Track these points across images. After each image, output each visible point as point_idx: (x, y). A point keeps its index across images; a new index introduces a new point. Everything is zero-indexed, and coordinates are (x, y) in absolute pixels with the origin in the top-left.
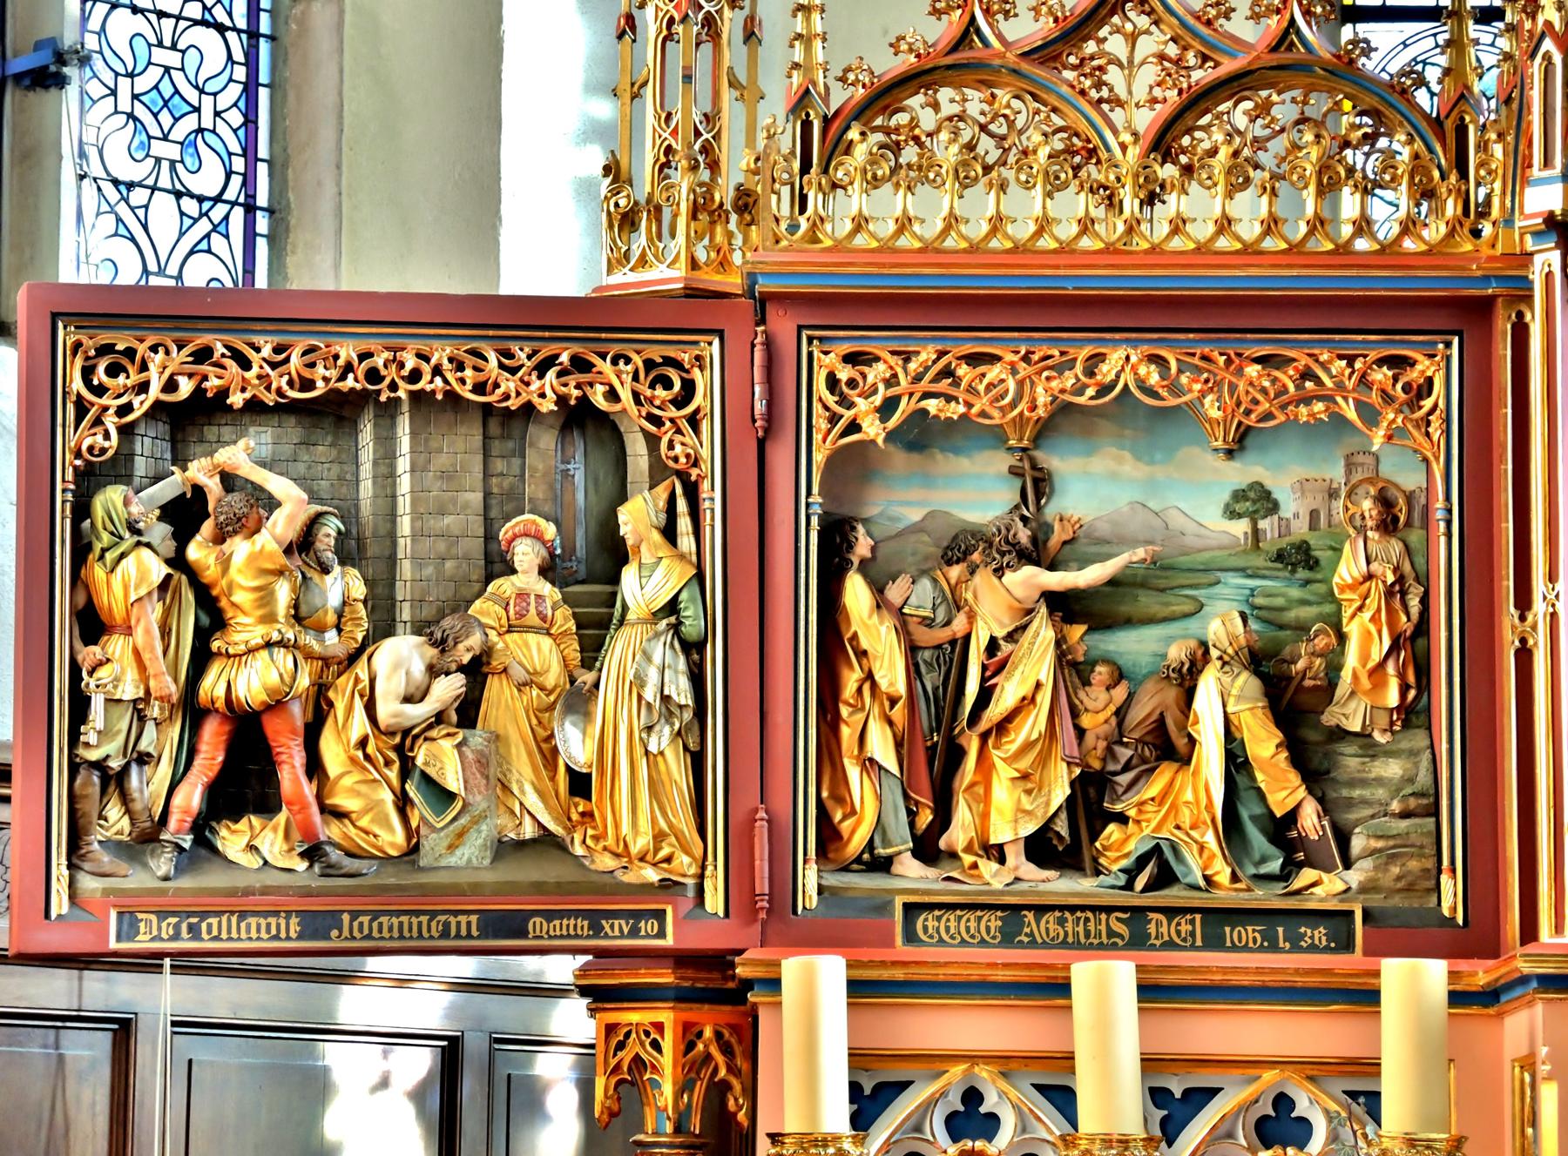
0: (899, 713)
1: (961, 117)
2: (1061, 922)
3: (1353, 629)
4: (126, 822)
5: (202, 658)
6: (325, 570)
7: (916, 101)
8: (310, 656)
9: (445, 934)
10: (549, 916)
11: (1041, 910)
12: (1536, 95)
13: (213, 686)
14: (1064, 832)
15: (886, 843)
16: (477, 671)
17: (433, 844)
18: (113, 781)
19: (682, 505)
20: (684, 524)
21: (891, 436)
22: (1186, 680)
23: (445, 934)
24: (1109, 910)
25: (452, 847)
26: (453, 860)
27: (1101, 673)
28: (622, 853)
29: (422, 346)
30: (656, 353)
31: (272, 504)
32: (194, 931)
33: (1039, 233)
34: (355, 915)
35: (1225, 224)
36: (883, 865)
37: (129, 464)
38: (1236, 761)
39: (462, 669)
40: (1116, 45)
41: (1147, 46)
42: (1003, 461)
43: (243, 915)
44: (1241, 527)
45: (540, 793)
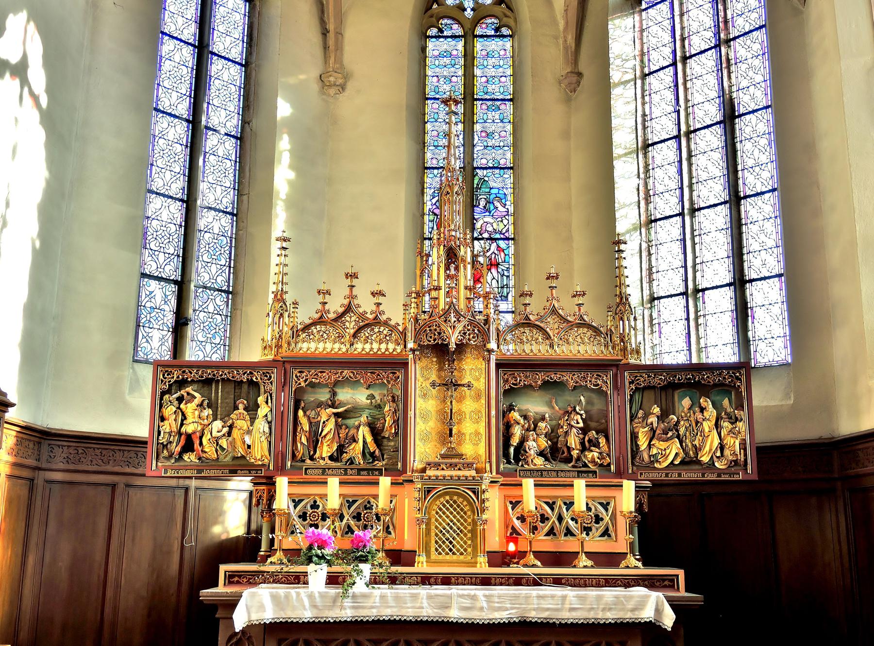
2: (332, 471)
3: (387, 419)
7: (313, 328)
8: (201, 424)
9: (222, 473)
10: (241, 470)
11: (329, 469)
16: (231, 427)
19: (269, 398)
24: (341, 469)
25: (225, 458)
38: (365, 442)
41: (353, 319)
42: (328, 390)
43: (186, 470)
44: (369, 401)
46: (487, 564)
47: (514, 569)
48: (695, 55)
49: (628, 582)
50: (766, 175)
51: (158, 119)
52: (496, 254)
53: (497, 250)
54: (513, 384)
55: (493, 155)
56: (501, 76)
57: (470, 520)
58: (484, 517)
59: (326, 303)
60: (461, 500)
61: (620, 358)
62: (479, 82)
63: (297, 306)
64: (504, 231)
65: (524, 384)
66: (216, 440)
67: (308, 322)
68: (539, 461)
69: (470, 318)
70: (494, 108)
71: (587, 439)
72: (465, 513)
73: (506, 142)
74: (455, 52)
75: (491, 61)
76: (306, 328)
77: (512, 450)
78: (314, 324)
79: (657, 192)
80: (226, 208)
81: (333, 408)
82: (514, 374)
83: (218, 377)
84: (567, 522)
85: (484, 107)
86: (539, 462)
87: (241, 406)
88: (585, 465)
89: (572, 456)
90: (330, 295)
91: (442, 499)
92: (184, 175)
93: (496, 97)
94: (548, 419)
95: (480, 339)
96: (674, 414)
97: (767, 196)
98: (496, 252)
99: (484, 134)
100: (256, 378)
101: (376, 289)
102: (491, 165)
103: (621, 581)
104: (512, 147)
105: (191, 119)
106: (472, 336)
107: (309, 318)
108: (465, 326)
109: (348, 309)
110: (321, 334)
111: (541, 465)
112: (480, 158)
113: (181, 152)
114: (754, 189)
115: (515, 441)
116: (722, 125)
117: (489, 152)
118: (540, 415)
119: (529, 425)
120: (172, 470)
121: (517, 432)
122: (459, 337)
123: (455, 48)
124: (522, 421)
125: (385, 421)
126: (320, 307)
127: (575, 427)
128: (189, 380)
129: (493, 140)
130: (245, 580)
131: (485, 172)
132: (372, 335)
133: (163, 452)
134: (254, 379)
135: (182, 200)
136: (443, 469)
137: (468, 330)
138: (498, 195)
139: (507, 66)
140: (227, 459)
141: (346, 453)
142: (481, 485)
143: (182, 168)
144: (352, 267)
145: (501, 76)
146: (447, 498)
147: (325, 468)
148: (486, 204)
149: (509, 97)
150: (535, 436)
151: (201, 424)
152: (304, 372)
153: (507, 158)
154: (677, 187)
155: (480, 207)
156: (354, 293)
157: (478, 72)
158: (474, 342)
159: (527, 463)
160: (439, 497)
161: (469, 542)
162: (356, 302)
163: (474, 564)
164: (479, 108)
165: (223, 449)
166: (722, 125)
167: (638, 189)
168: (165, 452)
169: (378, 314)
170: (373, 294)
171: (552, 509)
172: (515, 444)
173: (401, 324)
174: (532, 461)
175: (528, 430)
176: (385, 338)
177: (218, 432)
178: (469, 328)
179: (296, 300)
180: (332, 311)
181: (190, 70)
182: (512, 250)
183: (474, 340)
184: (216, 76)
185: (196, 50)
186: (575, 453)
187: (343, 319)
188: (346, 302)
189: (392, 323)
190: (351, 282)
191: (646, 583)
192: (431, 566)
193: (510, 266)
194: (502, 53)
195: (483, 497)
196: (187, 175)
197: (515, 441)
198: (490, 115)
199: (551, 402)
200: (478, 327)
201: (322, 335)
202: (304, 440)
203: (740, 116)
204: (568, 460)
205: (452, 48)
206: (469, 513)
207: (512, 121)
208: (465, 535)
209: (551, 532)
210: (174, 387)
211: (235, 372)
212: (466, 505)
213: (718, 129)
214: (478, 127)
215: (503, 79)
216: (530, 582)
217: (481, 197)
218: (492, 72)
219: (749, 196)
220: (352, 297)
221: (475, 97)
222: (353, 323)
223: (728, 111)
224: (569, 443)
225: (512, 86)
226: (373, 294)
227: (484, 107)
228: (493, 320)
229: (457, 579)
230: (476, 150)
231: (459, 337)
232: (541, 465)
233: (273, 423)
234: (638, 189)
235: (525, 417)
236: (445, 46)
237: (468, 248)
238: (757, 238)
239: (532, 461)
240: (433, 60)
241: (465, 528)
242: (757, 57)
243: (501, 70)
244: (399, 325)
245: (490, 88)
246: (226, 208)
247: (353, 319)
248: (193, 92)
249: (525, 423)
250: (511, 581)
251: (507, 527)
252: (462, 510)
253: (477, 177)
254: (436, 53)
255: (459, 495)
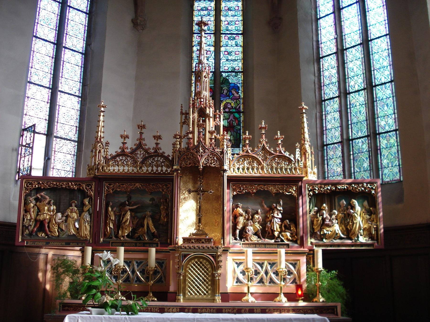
0: (113, 222)
1: (122, 159)
2: (128, 244)
3: (162, 213)
4: (28, 232)
5: (38, 215)
6: (51, 206)
7: (117, 158)
8: (49, 215)
9: (61, 245)
10: (73, 243)
11: (126, 243)
12: (177, 159)
13: (38, 218)
14: (130, 235)
15: (112, 236)
16: (67, 217)
17: (61, 235)
18: (27, 228)
19: (90, 200)
20: (90, 201)
21: (113, 192)
22: (144, 218)
23: (61, 245)
24: (133, 243)
25: (63, 235)
26: (63, 237)
27: (136, 218)
28: (81, 236)
29: (63, 182)
30: (88, 183)
31: (46, 199)
32: (34, 244)
33: (147, 172)
34: (52, 242)
35: (147, 170)
36: (111, 238)
37: (121, 244)
38: (148, 227)
39: (65, 216)
40: (139, 152)
41: (142, 152)
42: (126, 196)
43: (39, 242)
44: (151, 202)
45: (74, 230)
46: (220, 301)
47: (232, 304)
48: (345, 7)
49: (307, 311)
50: (387, 73)
51: (36, 42)
52: (233, 121)
53: (234, 118)
54: (239, 192)
55: (232, 64)
56: (236, 21)
57: (210, 274)
58: (219, 272)
59: (126, 143)
60: (205, 261)
61: (303, 175)
62: (223, 25)
63: (108, 145)
64: (238, 107)
65: (245, 191)
66: (58, 225)
67: (114, 154)
68: (254, 238)
69: (212, 150)
70: (232, 38)
71: (283, 225)
72: (207, 269)
73: (239, 57)
74: (210, 8)
75: (230, 13)
76: (114, 158)
77: (238, 232)
78: (118, 155)
79: (325, 84)
80: (75, 93)
81: (129, 206)
82: (239, 186)
83: (59, 187)
84: (270, 275)
85: (226, 38)
86: (255, 239)
87: (73, 205)
88: (282, 241)
89: (274, 235)
90: (128, 138)
91: (193, 261)
92: (51, 74)
93: (233, 32)
94: (260, 213)
95: (218, 163)
96: (335, 209)
97: (388, 85)
98: (233, 120)
99: (226, 53)
100: (83, 188)
101: (155, 134)
102: (230, 70)
103: (303, 311)
104: (242, 60)
105: (56, 43)
106: (213, 161)
107: (116, 152)
108: (208, 155)
109: (140, 146)
110: (122, 161)
111: (255, 241)
112: (224, 66)
113: (50, 62)
114: (380, 81)
115: (240, 226)
116: (362, 46)
117: (229, 63)
118: (255, 210)
119: (249, 217)
120: (31, 242)
121: (241, 220)
122: (205, 162)
123: (210, 5)
124: (244, 214)
125: (161, 214)
126: (122, 145)
127: (277, 218)
128: (42, 188)
129: (232, 56)
130: (72, 309)
131: (227, 74)
132: (153, 162)
133: (25, 231)
134: (81, 188)
135: (49, 88)
136: (192, 243)
137: (211, 158)
138: (234, 87)
139: (239, 16)
140: (64, 236)
141: (137, 233)
142: (217, 252)
143: (50, 70)
144: (142, 121)
145: (236, 21)
146: (196, 260)
147: (123, 242)
148: (227, 92)
149: (240, 32)
150: (252, 223)
151: (49, 215)
152: (111, 184)
153: (238, 66)
154: (336, 81)
155: (224, 94)
156: (143, 137)
157: (223, 18)
158: (214, 165)
159: (247, 240)
160: (191, 259)
161: (209, 287)
162: (144, 142)
163: (214, 300)
164: (223, 38)
165: (62, 230)
166: (362, 46)
167: (315, 83)
168: (27, 231)
169: (156, 150)
170: (154, 137)
171: (262, 267)
172: (240, 228)
173: (171, 155)
174: (250, 238)
175: (248, 220)
176: (161, 164)
177: (59, 220)
178: (211, 156)
179: (107, 141)
180: (129, 147)
181: (56, 15)
182: (242, 119)
183: (214, 163)
184: (71, 19)
185: (61, 5)
186: (276, 234)
187: (136, 153)
188: (138, 142)
189: (166, 155)
190: (141, 130)
191: (318, 311)
192: (186, 302)
193: (241, 128)
194: (237, 8)
195: (218, 260)
196: (52, 73)
197: (240, 226)
198: (230, 42)
199: (262, 202)
200: (217, 156)
201: (123, 162)
202: (111, 226)
203: (371, 40)
204: (272, 237)
205: (208, 5)
206: (210, 269)
207: (242, 46)
208: (207, 283)
209: (261, 281)
210: (33, 192)
211: (70, 184)
212: (208, 265)
213: (360, 48)
214: (223, 49)
215: (237, 23)
216: (247, 311)
217: (224, 88)
218: (230, 19)
219: (378, 85)
220: (141, 139)
221: (221, 32)
222: (142, 155)
223: (364, 38)
224: (272, 227)
225: (242, 26)
226: (154, 137)
227: (226, 38)
228: (225, 152)
229: (202, 310)
230: (221, 62)
231: (205, 162)
232: (255, 241)
233: (92, 215)
234: (315, 83)
235: (247, 212)
236: (204, 5)
237: (211, 108)
238: (374, 18)
239: (250, 238)
240: (197, 12)
241: (207, 278)
242: (389, 98)
243: (236, 17)
244: (170, 156)
245: (230, 27)
246: (75, 93)
247: (142, 152)
248: (58, 27)
249: (246, 216)
250: (235, 311)
251: (234, 278)
252: (205, 267)
253: (222, 77)
254: (199, 8)
255: (204, 258)
